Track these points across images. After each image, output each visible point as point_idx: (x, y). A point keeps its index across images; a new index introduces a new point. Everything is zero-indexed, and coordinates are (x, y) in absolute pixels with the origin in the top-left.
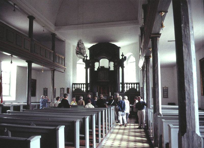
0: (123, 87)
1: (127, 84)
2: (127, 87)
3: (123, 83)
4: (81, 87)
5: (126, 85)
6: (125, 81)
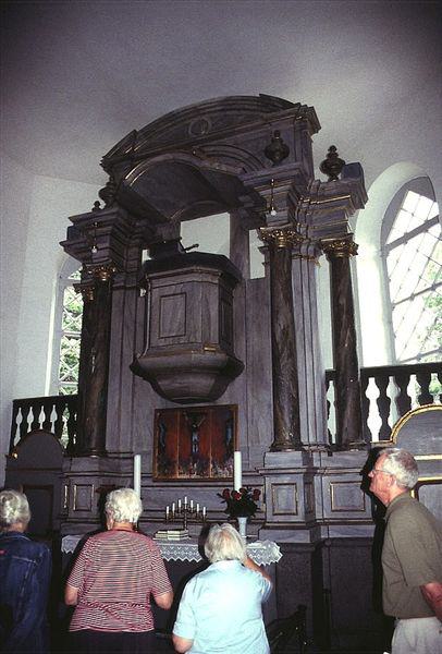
0: (352, 409)
1: (381, 375)
2: (384, 403)
3: (348, 375)
4: (59, 423)
5: (372, 392)
6: (372, 353)
